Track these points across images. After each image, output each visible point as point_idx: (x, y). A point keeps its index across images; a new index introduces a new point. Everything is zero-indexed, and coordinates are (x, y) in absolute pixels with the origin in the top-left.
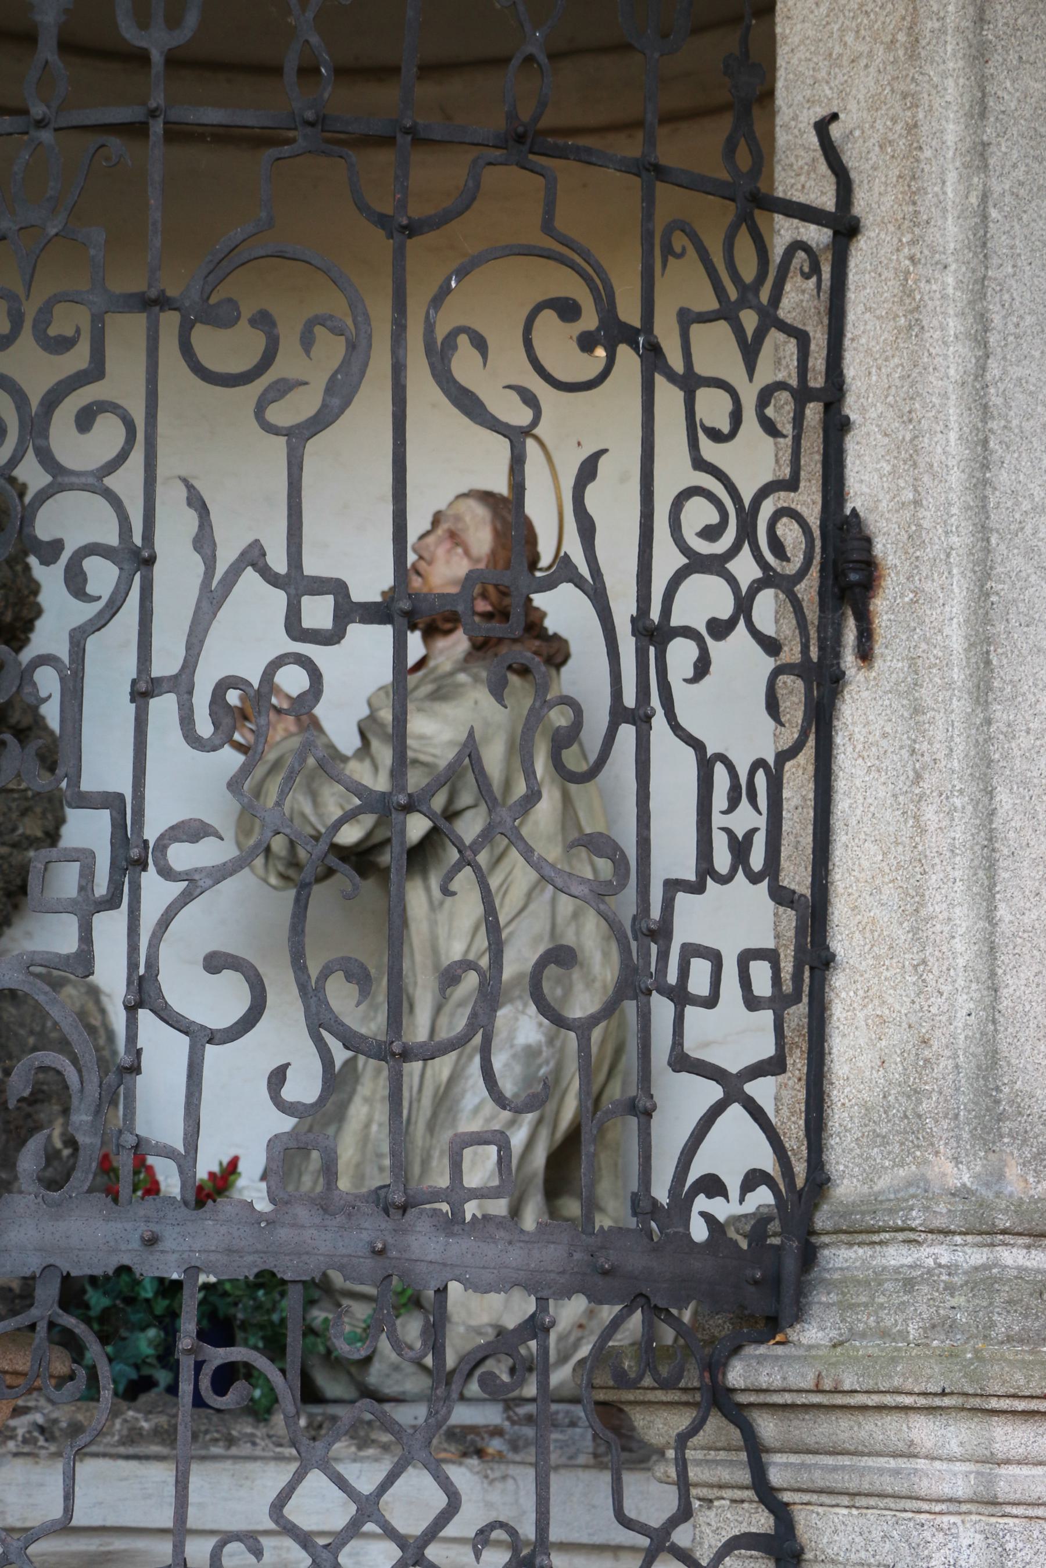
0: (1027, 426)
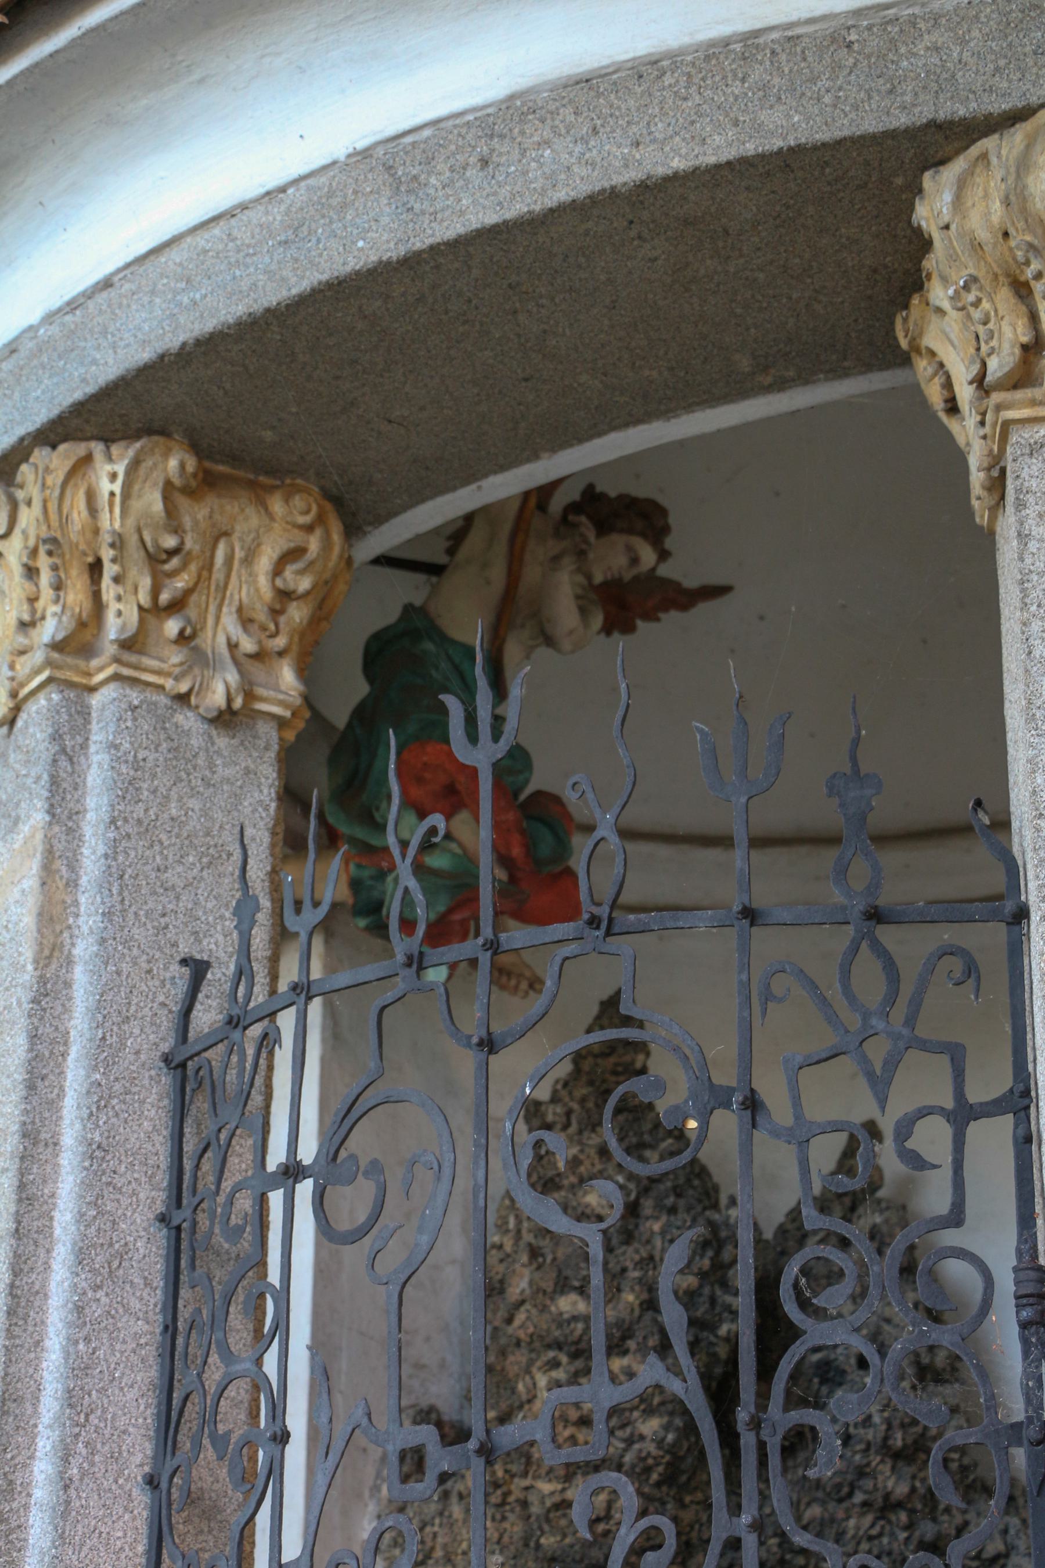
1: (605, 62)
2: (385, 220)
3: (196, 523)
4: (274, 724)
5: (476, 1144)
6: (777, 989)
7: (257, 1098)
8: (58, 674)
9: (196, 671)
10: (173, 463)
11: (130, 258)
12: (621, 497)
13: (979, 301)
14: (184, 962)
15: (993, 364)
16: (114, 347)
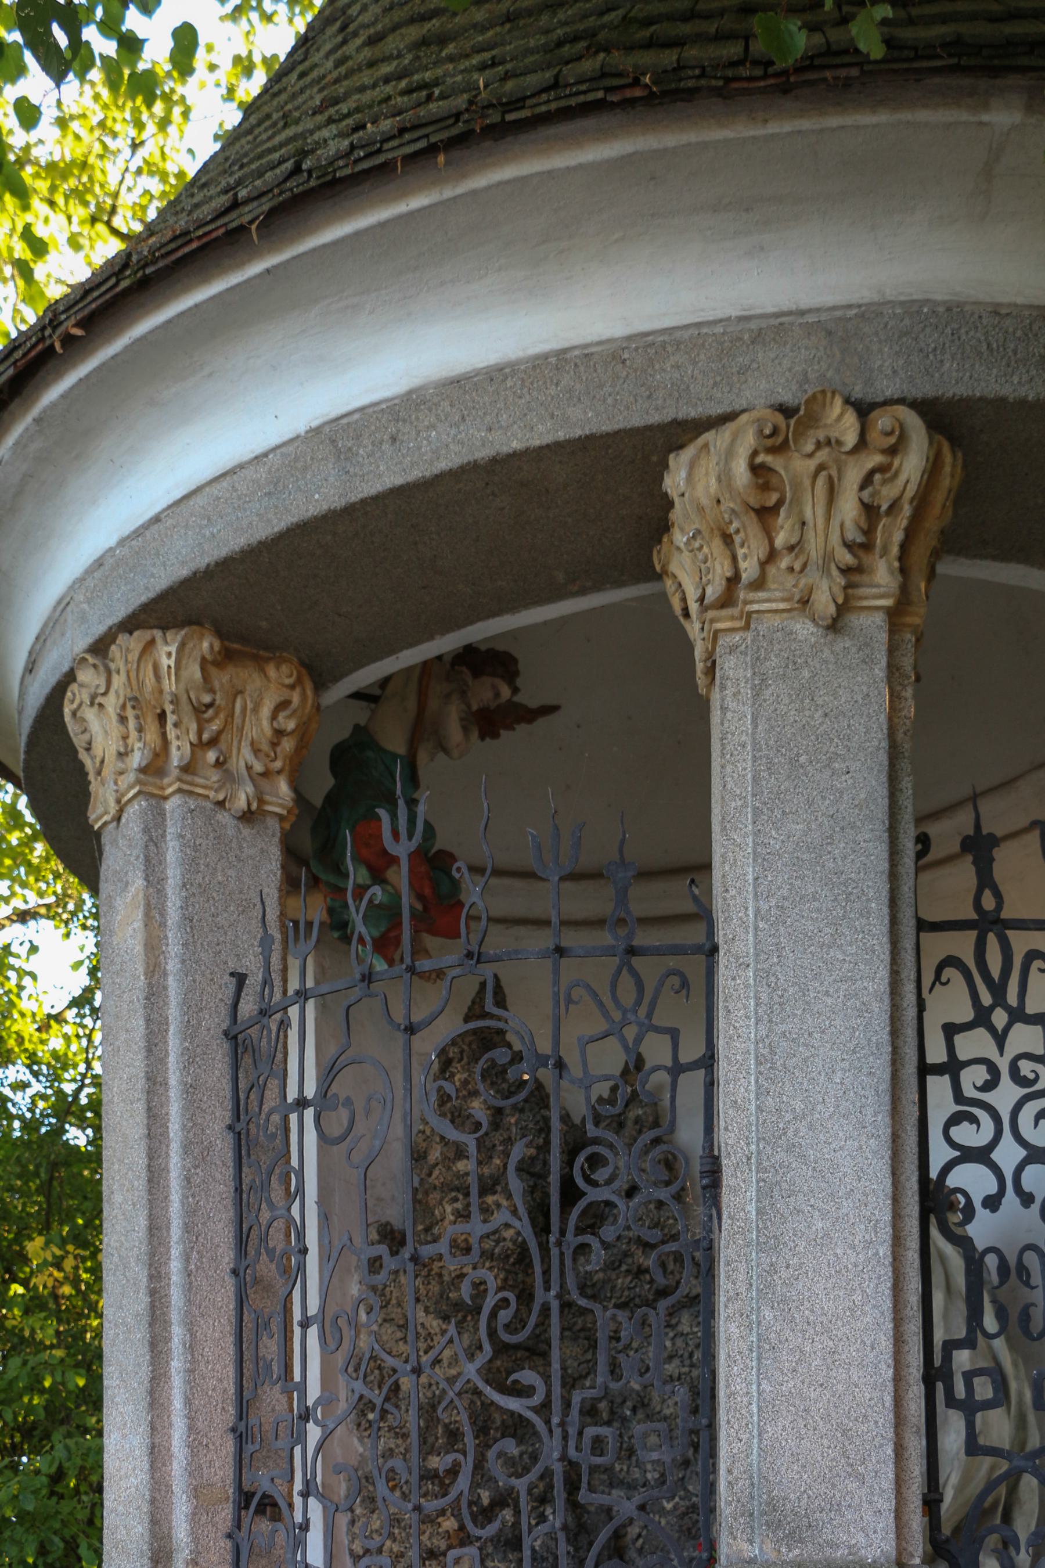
0: (790, 1063)
1: (469, 368)
2: (332, 479)
3: (222, 685)
4: (277, 819)
5: (405, 1088)
6: (575, 997)
7: (279, 1056)
8: (145, 789)
9: (228, 786)
10: (206, 645)
11: (171, 502)
12: (488, 651)
13: (701, 547)
14: (232, 974)
15: (709, 591)
16: (164, 564)
